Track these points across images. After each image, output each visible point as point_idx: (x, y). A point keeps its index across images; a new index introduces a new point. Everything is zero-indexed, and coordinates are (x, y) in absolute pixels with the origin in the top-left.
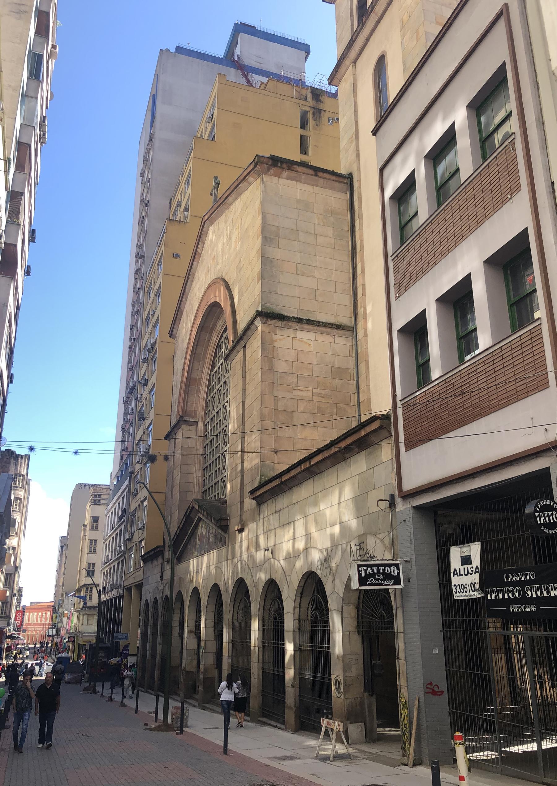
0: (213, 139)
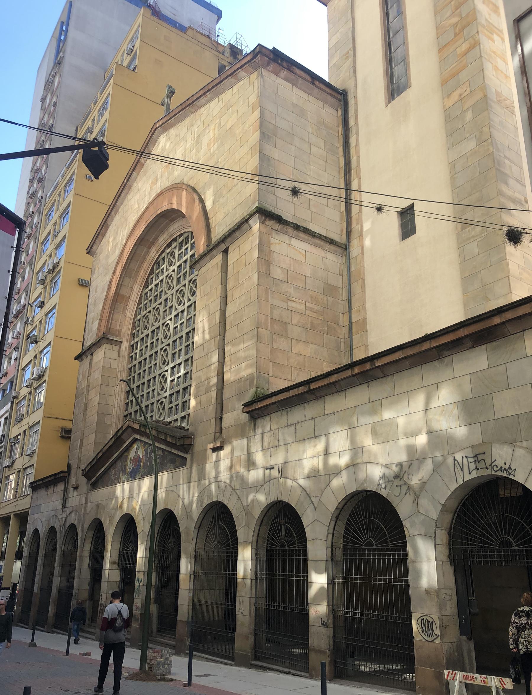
0: (134, 70)
